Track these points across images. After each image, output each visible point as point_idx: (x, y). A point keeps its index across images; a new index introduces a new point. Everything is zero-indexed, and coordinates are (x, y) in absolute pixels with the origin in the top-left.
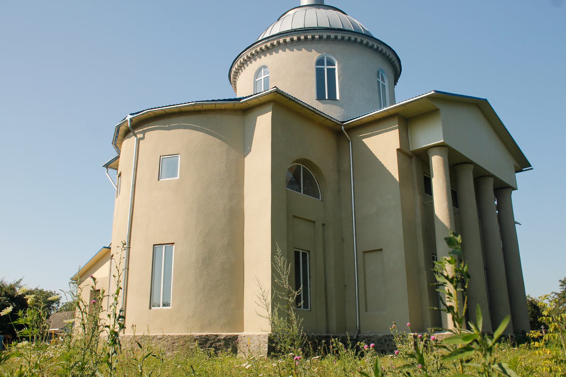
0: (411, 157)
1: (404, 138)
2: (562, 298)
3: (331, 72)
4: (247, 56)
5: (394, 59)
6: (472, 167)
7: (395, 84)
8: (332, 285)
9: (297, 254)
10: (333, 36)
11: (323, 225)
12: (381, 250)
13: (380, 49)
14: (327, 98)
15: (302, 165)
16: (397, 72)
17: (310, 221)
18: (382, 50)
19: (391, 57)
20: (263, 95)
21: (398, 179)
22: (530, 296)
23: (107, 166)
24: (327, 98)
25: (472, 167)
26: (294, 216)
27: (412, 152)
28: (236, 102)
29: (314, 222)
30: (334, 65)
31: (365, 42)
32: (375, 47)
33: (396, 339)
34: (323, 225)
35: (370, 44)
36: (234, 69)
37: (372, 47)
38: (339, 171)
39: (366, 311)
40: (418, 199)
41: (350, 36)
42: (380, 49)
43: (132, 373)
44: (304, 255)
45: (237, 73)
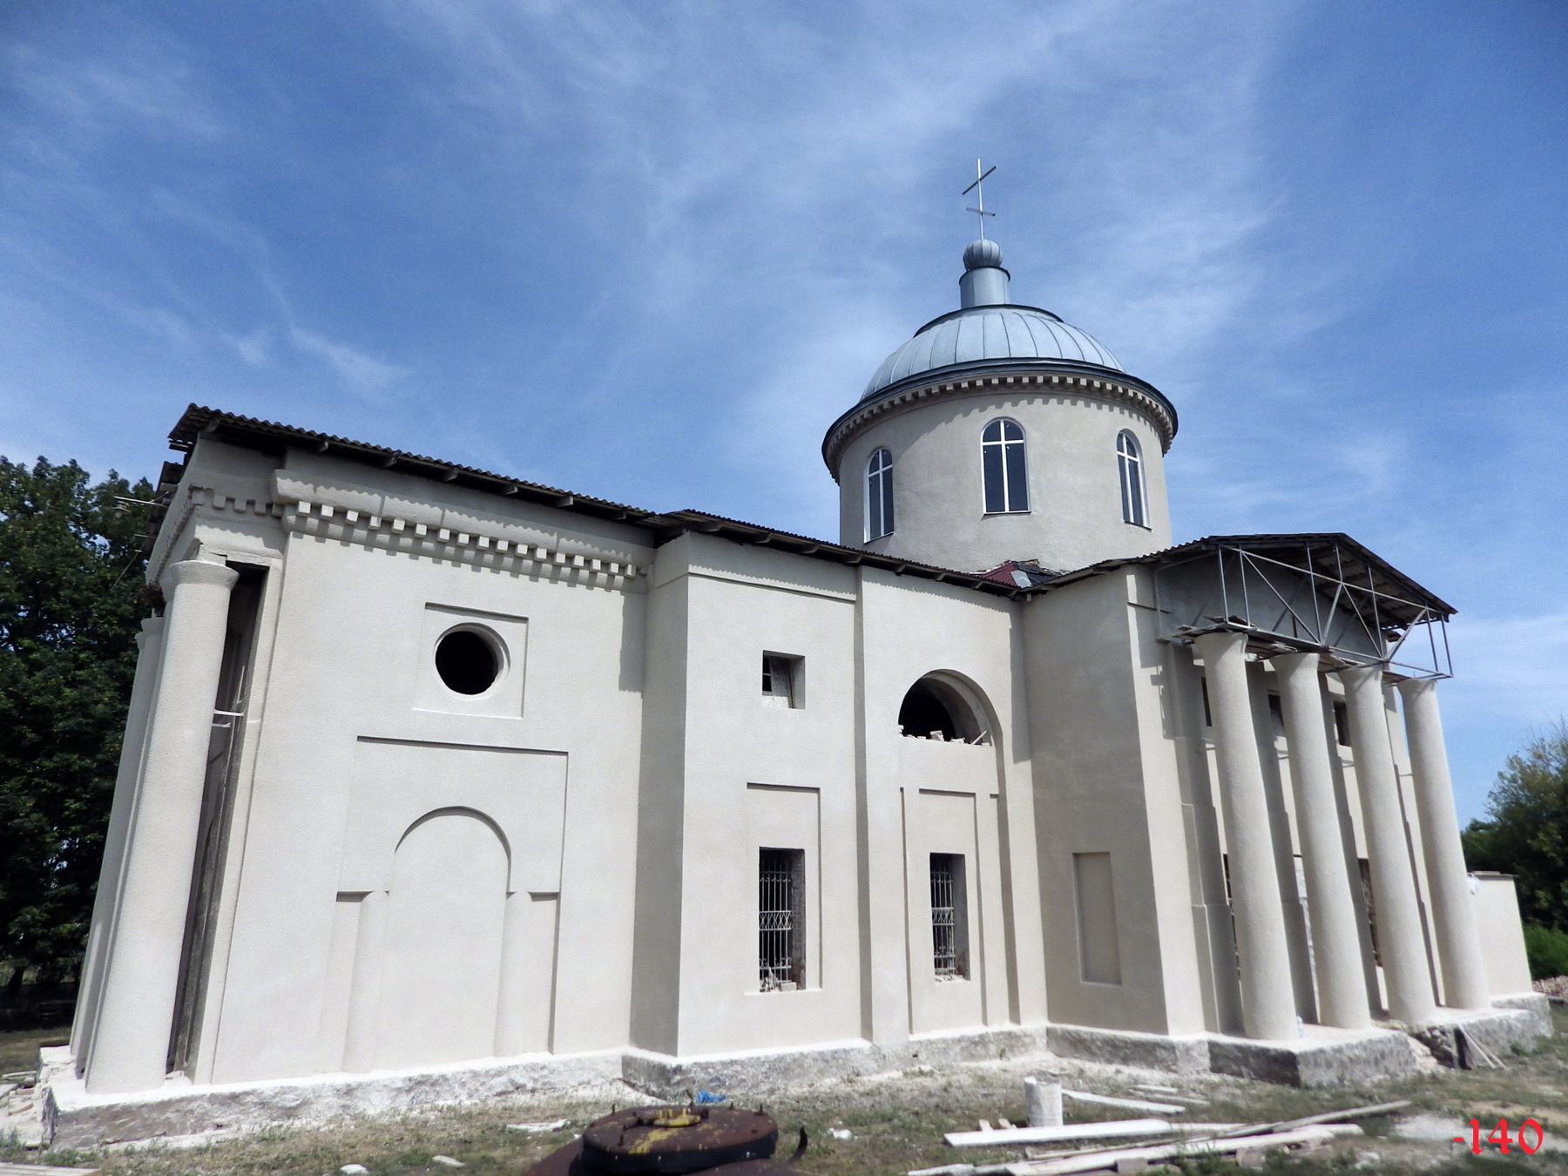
3: (1017, 454)
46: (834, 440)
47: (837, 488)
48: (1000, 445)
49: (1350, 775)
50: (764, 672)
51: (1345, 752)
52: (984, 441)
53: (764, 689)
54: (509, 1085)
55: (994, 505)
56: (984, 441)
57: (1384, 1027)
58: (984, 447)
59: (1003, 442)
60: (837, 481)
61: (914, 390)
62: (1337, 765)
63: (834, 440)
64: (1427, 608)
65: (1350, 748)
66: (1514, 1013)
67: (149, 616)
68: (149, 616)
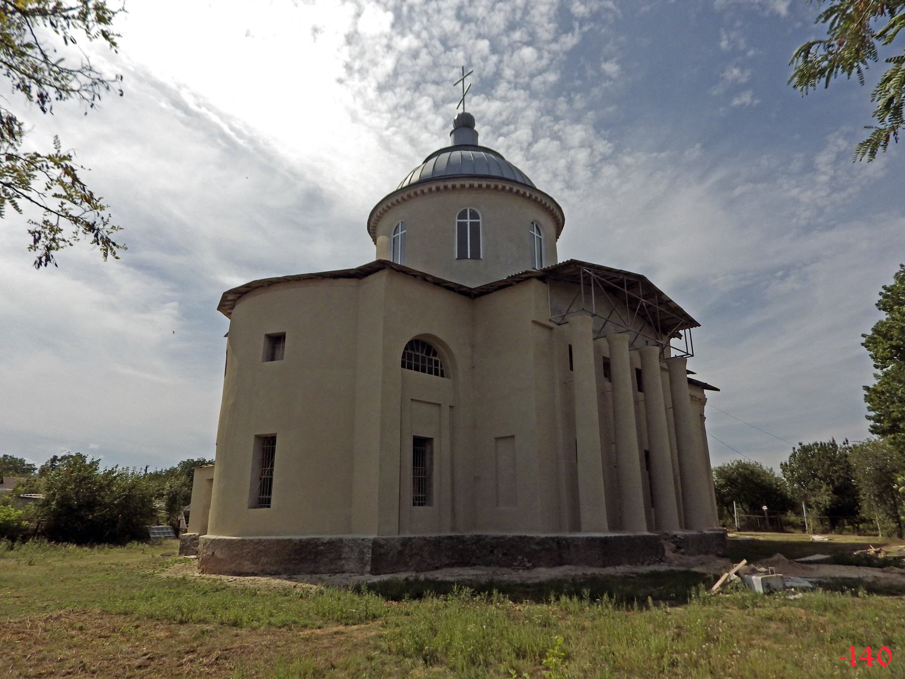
2: (552, 622)
3: (475, 228)
4: (383, 209)
5: (552, 207)
7: (557, 237)
10: (476, 183)
13: (534, 197)
14: (469, 257)
16: (559, 223)
17: (437, 404)
18: (546, 203)
19: (548, 205)
20: (675, 448)
23: (450, 406)
24: (469, 257)
29: (439, 405)
30: (479, 219)
31: (515, 190)
32: (528, 195)
35: (522, 192)
37: (524, 195)
42: (534, 197)
43: (599, 640)
46: (375, 217)
47: (376, 248)
48: (467, 219)
49: (642, 404)
50: (402, 358)
51: (641, 394)
52: (479, 222)
53: (402, 367)
54: (495, 599)
55: (462, 256)
56: (479, 222)
57: (879, 571)
58: (458, 223)
59: (468, 221)
60: (375, 244)
61: (525, 191)
62: (636, 402)
63: (375, 217)
64: (683, 321)
65: (228, 321)
66: (788, 530)
67: (784, 467)
68: (784, 467)
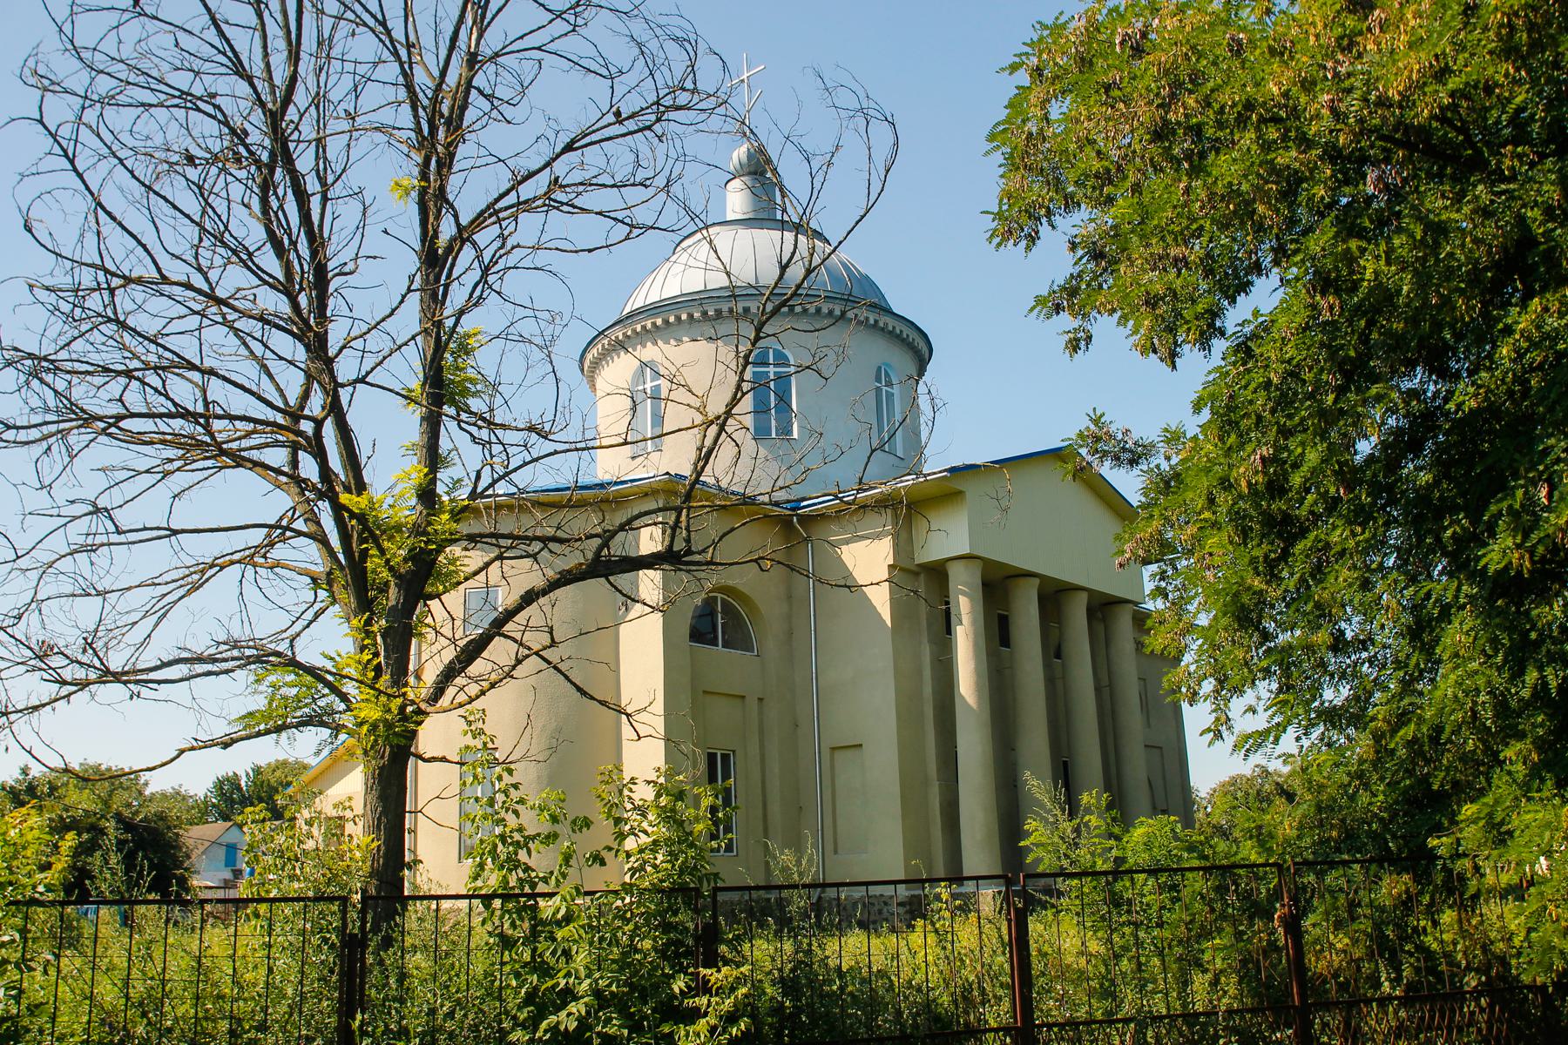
0: (917, 574)
1: (903, 547)
6: (1037, 581)
8: (775, 808)
9: (711, 758)
11: (760, 700)
12: (861, 745)
15: (719, 595)
21: (889, 623)
22: (1214, 786)
25: (1037, 581)
26: (705, 692)
27: (919, 565)
28: (407, 826)
29: (743, 697)
33: (1502, 850)
34: (760, 700)
36: (589, 357)
38: (789, 597)
39: (836, 852)
40: (926, 651)
41: (831, 306)
44: (725, 758)
45: (596, 364)
